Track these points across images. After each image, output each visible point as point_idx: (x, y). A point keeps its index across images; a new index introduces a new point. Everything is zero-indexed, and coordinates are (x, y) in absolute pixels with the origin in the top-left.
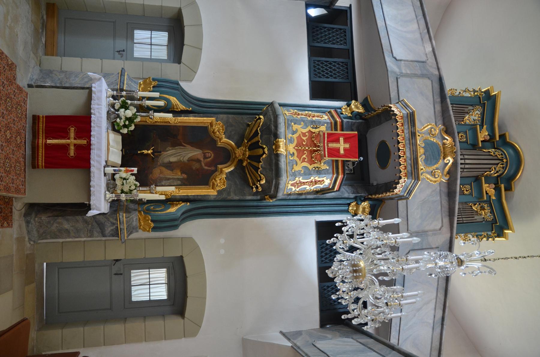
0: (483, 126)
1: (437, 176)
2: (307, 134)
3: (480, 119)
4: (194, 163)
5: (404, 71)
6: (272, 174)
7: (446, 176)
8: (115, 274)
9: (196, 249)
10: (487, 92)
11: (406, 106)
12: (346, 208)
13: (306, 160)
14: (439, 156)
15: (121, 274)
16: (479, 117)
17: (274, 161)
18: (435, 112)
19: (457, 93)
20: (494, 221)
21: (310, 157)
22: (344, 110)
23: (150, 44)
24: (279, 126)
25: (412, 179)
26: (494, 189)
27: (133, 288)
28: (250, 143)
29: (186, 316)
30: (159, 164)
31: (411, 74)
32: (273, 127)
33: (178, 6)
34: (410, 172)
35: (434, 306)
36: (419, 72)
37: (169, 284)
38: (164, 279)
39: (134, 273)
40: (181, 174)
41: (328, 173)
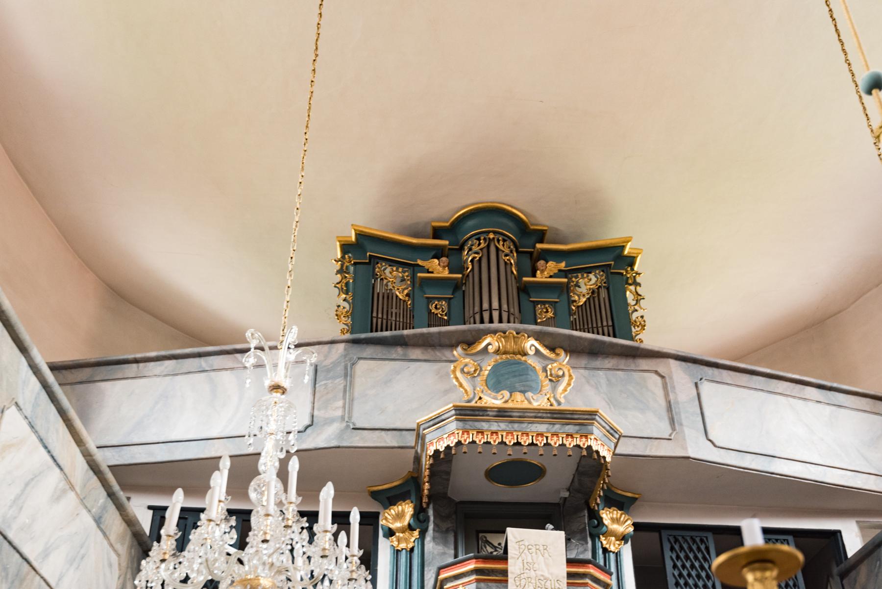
0: (418, 265)
1: (561, 373)
3: (400, 270)
5: (339, 413)
10: (346, 248)
11: (437, 421)
12: (612, 556)
14: (519, 363)
16: (397, 270)
18: (425, 361)
19: (346, 305)
20: (605, 268)
22: (403, 545)
25: (592, 424)
26: (547, 262)
31: (344, 398)
34: (577, 428)
35: (801, 401)
36: (340, 382)
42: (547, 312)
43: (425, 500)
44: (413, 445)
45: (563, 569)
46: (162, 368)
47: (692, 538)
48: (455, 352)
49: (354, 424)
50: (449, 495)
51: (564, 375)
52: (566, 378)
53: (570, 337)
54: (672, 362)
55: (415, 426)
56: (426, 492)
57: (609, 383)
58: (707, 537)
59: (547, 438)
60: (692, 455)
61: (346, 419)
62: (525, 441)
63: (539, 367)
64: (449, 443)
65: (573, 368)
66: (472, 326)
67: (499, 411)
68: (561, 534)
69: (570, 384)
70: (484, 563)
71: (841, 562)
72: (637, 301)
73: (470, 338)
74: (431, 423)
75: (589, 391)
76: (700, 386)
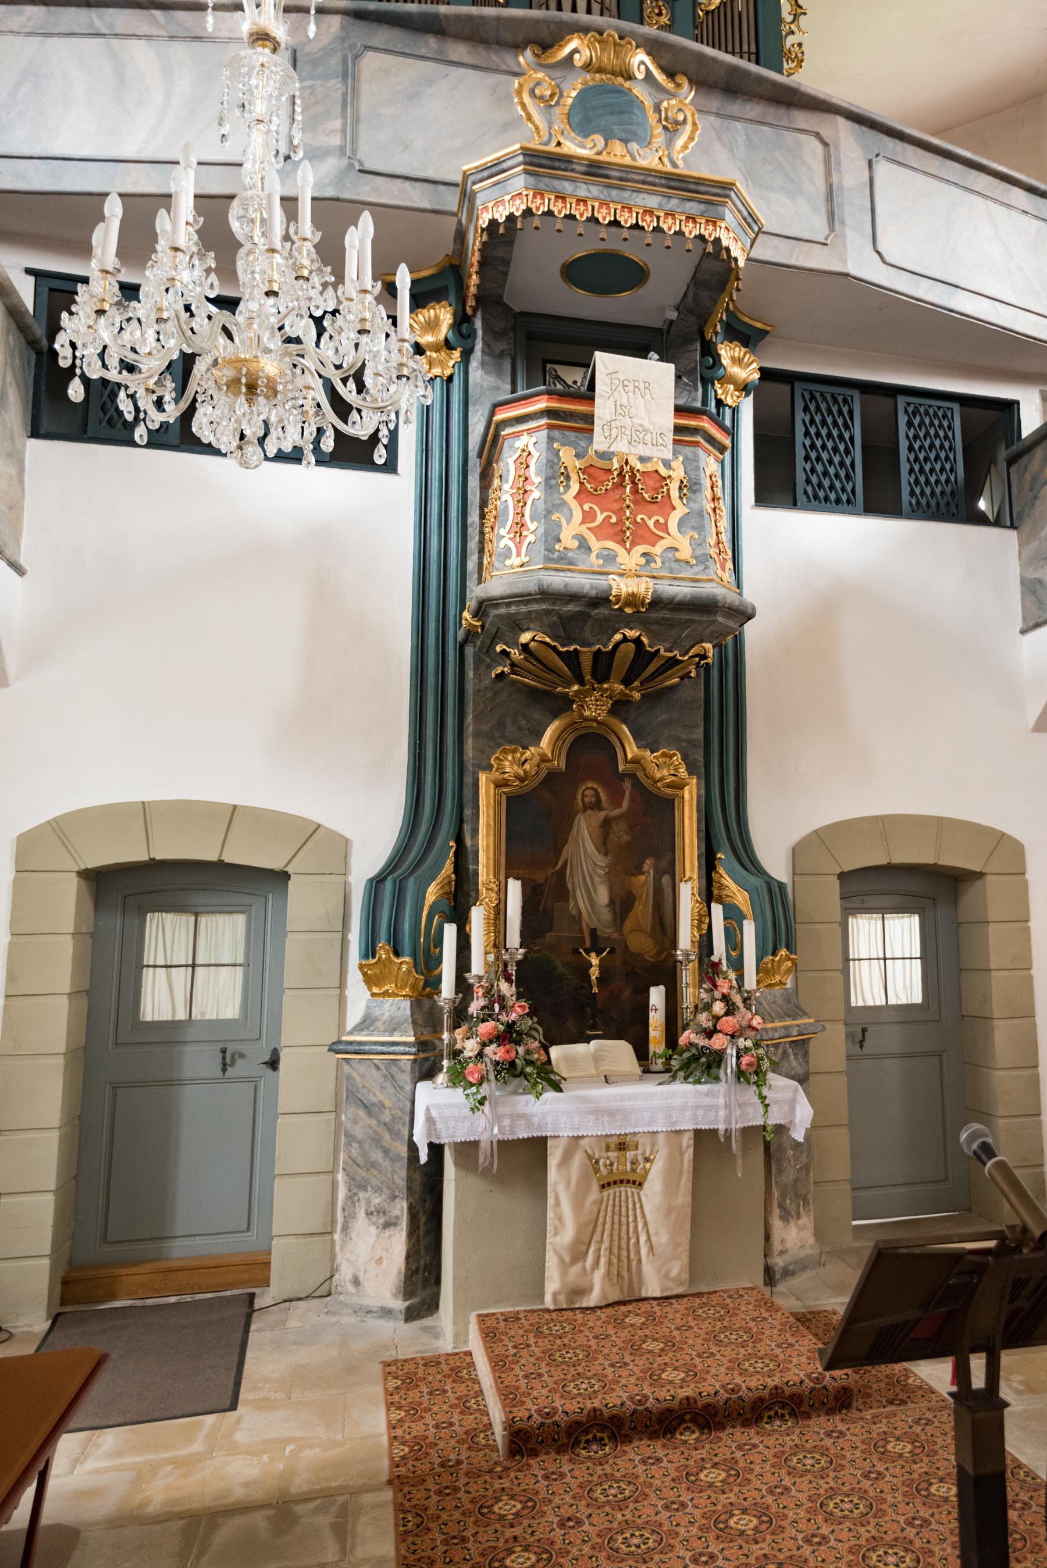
1: (681, 117)
2: (586, 507)
4: (612, 837)
5: (336, 141)
6: (699, 623)
7: (678, 85)
8: (861, 1047)
9: (822, 839)
11: (494, 169)
12: (728, 412)
13: (662, 520)
14: (620, 91)
15: (864, 1030)
17: (666, 614)
18: (474, 67)
21: (653, 507)
22: (437, 371)
23: (192, 972)
24: (574, 589)
25: (724, 204)
27: (893, 1001)
28: (588, 677)
29: (978, 870)
30: (616, 935)
31: (344, 116)
32: (571, 607)
33: (74, 881)
34: (703, 207)
35: (1002, 208)
36: (335, 85)
37: (883, 911)
38: (873, 922)
39: (857, 1000)
40: (642, 873)
41: (696, 459)
42: (660, 14)
43: (471, 302)
44: (455, 209)
45: (668, 420)
46: (22, 19)
47: (833, 396)
48: (521, 59)
49: (361, 163)
50: (505, 300)
51: (685, 121)
52: (689, 127)
53: (700, 56)
54: (841, 120)
55: (458, 178)
56: (473, 290)
57: (750, 145)
58: (852, 397)
59: (658, 218)
60: (853, 272)
61: (348, 153)
62: (627, 219)
63: (648, 103)
64: (513, 210)
65: (699, 111)
66: (553, 13)
67: (590, 166)
68: (670, 368)
69: (694, 138)
70: (560, 401)
71: (1013, 444)
72: (796, 17)
73: (545, 35)
74: (486, 173)
75: (721, 154)
76: (875, 166)
